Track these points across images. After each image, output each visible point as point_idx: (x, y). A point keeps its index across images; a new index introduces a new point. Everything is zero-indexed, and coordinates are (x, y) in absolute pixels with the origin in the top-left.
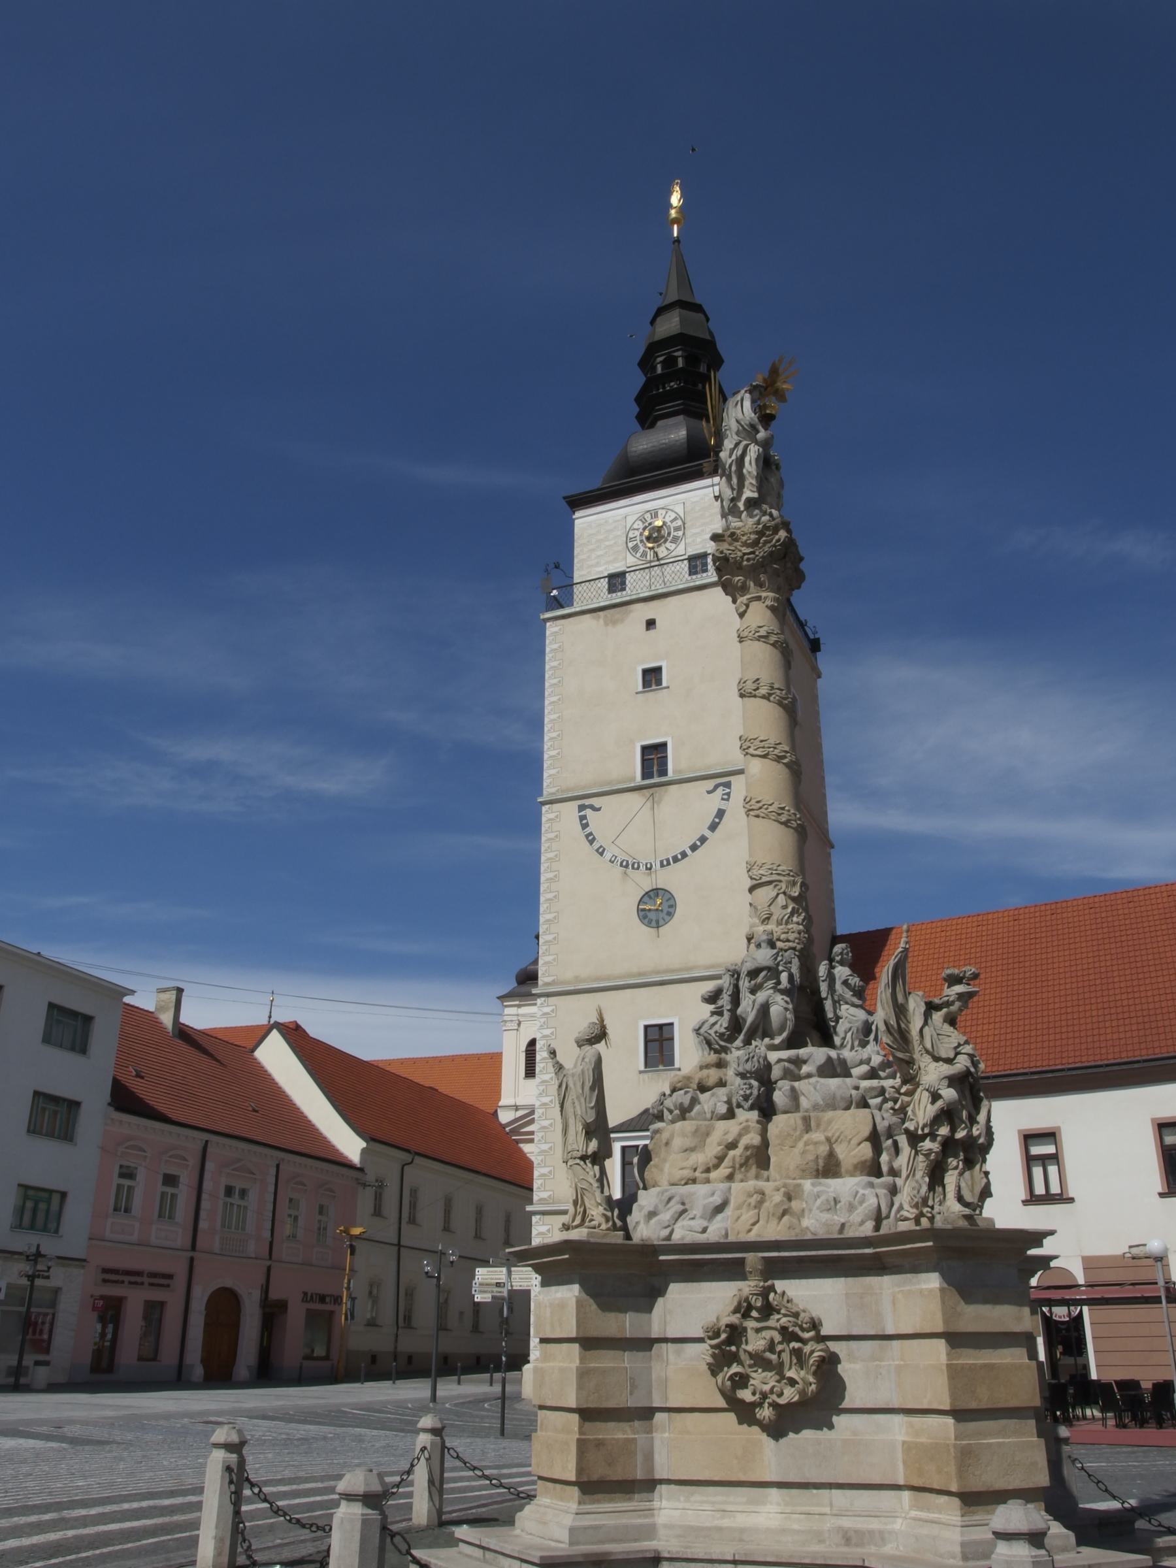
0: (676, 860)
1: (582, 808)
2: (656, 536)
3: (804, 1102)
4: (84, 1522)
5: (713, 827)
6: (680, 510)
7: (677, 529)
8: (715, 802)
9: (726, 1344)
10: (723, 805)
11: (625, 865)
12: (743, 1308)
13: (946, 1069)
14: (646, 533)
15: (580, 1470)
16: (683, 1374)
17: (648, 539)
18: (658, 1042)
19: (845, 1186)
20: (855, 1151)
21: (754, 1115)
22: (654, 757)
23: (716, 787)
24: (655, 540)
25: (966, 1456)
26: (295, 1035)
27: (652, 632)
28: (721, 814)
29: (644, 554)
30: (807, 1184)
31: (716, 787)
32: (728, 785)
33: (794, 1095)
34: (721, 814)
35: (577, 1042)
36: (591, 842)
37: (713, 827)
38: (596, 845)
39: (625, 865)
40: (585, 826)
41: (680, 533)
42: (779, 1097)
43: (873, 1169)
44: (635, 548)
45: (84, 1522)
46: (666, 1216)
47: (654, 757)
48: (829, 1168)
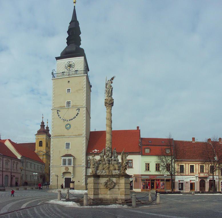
0: (71, 120)
1: (57, 111)
2: (70, 66)
3: (112, 163)
4: (52, 197)
5: (77, 115)
6: (74, 62)
7: (73, 65)
8: (77, 112)
9: (106, 184)
10: (78, 112)
11: (64, 120)
12: (108, 181)
13: (125, 162)
14: (69, 65)
15: (125, 182)
16: (102, 186)
17: (69, 66)
18: (192, 185)
19: (117, 171)
20: (117, 168)
21: (108, 164)
22: (68, 103)
23: (78, 109)
24: (70, 67)
25: (125, 192)
26: (10, 140)
27: (69, 83)
28: (78, 113)
29: (68, 69)
30: (113, 171)
31: (78, 109)
32: (79, 109)
33: (112, 163)
34: (78, 113)
35: (41, 141)
36: (59, 116)
37: (77, 115)
38: (60, 117)
39: (64, 120)
40: (58, 114)
41: (74, 66)
42: (110, 163)
43: (118, 170)
44: (67, 68)
45: (52, 197)
46: (100, 173)
47: (68, 103)
48: (115, 170)
